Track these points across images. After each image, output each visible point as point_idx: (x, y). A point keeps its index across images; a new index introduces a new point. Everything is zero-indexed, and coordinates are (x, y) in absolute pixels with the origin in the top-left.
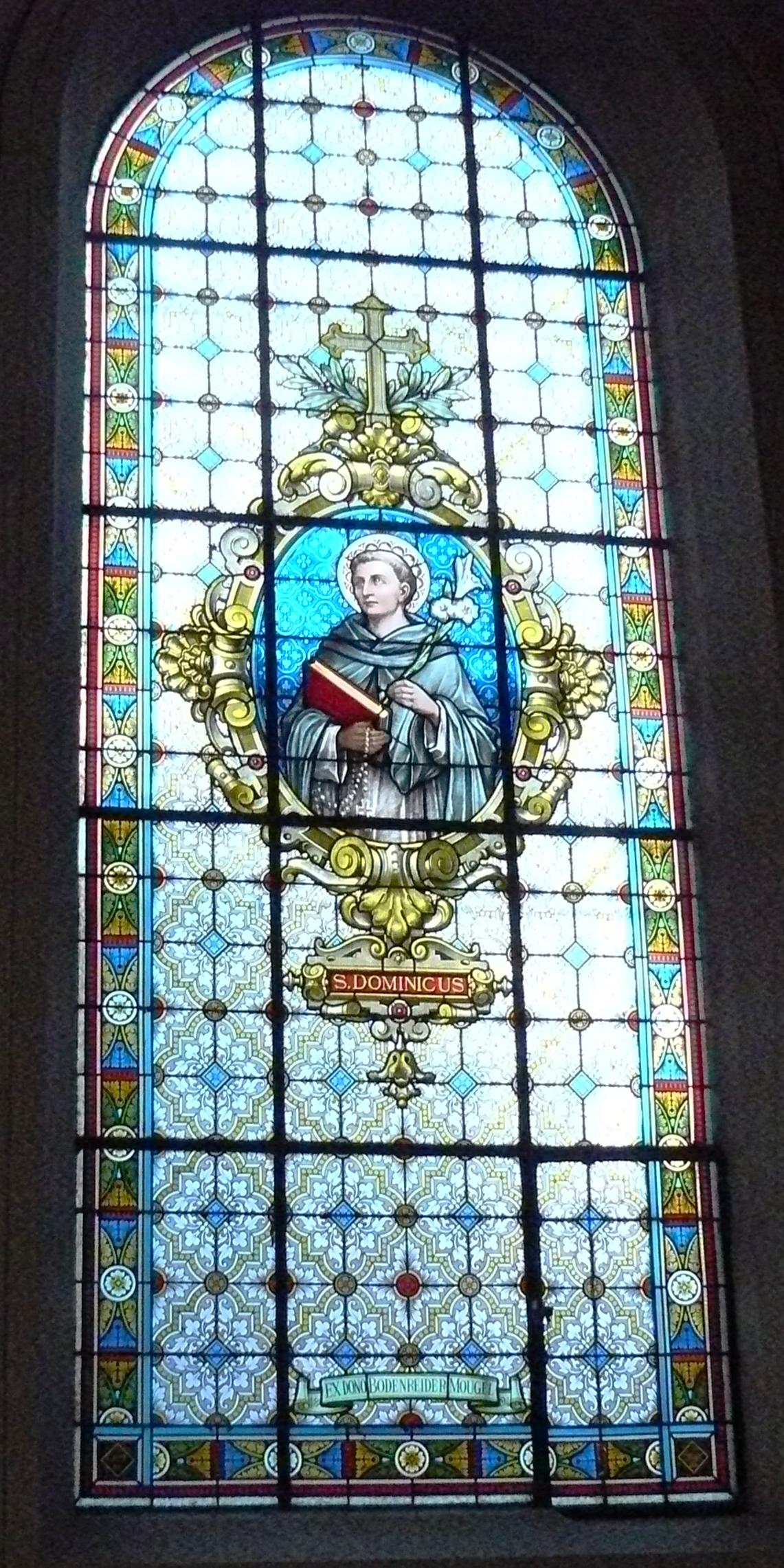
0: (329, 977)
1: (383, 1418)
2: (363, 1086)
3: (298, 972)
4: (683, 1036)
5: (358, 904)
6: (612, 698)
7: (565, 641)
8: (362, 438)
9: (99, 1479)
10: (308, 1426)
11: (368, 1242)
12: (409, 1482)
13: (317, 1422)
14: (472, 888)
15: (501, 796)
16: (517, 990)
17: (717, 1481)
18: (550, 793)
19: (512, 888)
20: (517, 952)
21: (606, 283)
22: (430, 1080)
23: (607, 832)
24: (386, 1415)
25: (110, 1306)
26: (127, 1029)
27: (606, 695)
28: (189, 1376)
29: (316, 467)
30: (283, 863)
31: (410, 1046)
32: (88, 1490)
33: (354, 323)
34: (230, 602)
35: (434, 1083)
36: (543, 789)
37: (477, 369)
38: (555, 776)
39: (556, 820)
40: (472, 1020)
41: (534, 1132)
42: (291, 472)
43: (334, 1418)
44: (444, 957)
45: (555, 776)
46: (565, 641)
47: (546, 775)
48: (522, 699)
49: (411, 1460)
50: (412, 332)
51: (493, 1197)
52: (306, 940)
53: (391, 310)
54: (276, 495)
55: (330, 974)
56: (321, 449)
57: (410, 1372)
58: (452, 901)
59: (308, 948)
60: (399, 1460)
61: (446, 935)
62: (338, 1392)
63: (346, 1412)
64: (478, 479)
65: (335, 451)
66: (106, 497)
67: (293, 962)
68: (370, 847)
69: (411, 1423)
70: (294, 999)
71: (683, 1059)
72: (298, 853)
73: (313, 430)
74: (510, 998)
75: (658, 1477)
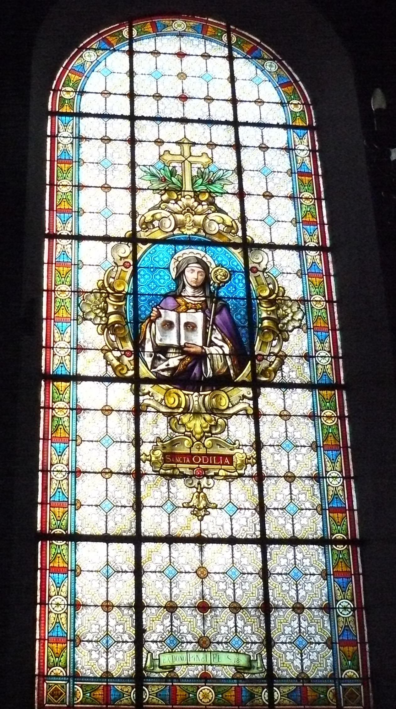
6: (304, 322)
7: (281, 294)
13: (157, 675)
14: (236, 414)
27: (301, 320)
29: (158, 216)
33: (176, 149)
36: (270, 365)
48: (259, 323)
54: (138, 228)
57: (205, 651)
60: (200, 695)
61: (224, 435)
62: (166, 660)
63: (172, 671)
69: (205, 678)
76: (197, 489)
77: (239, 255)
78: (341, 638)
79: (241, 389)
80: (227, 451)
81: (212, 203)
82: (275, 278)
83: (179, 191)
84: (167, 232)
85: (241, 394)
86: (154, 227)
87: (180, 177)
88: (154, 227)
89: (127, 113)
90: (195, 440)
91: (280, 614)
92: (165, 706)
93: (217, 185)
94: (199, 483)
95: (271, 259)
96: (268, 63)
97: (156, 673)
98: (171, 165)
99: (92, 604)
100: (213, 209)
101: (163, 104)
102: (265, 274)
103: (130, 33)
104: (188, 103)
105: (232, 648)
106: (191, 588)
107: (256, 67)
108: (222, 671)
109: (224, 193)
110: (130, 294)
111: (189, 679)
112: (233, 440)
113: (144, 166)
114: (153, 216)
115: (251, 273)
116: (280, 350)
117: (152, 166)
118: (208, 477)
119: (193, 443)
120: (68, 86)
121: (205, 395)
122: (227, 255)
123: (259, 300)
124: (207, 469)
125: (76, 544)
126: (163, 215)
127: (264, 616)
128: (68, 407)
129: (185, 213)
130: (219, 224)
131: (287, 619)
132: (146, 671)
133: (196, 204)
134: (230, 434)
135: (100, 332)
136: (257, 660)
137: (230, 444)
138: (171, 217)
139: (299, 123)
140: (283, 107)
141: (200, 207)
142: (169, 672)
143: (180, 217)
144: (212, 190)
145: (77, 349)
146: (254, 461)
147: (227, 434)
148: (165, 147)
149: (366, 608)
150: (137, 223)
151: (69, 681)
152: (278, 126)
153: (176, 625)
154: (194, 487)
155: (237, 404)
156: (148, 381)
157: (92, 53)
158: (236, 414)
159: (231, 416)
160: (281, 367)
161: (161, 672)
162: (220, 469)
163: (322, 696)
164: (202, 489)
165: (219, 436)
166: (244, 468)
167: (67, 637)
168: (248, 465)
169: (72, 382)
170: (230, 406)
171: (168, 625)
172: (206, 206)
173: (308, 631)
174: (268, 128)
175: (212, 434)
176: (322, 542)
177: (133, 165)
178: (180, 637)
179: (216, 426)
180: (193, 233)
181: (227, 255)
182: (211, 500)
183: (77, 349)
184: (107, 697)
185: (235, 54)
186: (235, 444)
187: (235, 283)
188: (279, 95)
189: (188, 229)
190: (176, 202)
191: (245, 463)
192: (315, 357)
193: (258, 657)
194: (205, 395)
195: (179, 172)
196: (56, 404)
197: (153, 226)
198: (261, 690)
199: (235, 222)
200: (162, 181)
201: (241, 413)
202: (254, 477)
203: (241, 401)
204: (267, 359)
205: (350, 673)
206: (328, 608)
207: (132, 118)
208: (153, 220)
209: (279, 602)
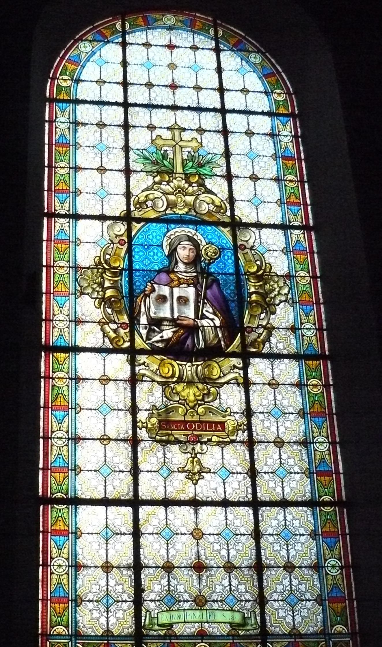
6: (290, 296)
7: (268, 270)
8: (171, 184)
13: (155, 633)
14: (228, 383)
20: (249, 413)
24: (192, 629)
29: (151, 197)
33: (167, 134)
36: (259, 337)
42: (139, 198)
54: (132, 208)
59: (149, 410)
61: (216, 403)
62: (164, 618)
76: (191, 454)
77: (227, 233)
80: (219, 418)
81: (202, 185)
82: (262, 255)
84: (160, 212)
85: (232, 364)
86: (147, 207)
88: (147, 207)
89: (121, 100)
90: (188, 408)
93: (206, 168)
94: (193, 449)
95: (258, 237)
97: (155, 631)
98: (163, 149)
99: (92, 565)
100: (202, 191)
102: (253, 252)
108: (218, 628)
109: (213, 176)
112: (225, 408)
114: (146, 196)
115: (239, 251)
116: (268, 323)
117: (145, 150)
119: (187, 410)
122: (216, 233)
124: (201, 435)
125: (76, 508)
126: (156, 196)
130: (208, 204)
133: (186, 185)
136: (251, 617)
137: (222, 411)
139: (282, 111)
140: (267, 96)
141: (191, 188)
142: (167, 630)
143: (172, 198)
147: (219, 402)
148: (157, 132)
149: (353, 566)
150: (132, 203)
151: (71, 640)
152: (263, 113)
153: (173, 585)
154: (188, 452)
156: (143, 352)
157: (87, 44)
158: (228, 383)
159: (222, 384)
161: (160, 630)
164: (196, 454)
165: (211, 404)
166: (236, 434)
170: (222, 375)
172: (196, 188)
174: (254, 116)
175: (205, 402)
177: (127, 148)
179: (209, 394)
180: (184, 213)
182: (205, 464)
185: (222, 46)
186: (226, 411)
194: (198, 365)
197: (147, 205)
199: (224, 202)
201: (232, 382)
203: (232, 371)
204: (255, 332)
205: (340, 628)
208: (147, 201)
209: (271, 562)
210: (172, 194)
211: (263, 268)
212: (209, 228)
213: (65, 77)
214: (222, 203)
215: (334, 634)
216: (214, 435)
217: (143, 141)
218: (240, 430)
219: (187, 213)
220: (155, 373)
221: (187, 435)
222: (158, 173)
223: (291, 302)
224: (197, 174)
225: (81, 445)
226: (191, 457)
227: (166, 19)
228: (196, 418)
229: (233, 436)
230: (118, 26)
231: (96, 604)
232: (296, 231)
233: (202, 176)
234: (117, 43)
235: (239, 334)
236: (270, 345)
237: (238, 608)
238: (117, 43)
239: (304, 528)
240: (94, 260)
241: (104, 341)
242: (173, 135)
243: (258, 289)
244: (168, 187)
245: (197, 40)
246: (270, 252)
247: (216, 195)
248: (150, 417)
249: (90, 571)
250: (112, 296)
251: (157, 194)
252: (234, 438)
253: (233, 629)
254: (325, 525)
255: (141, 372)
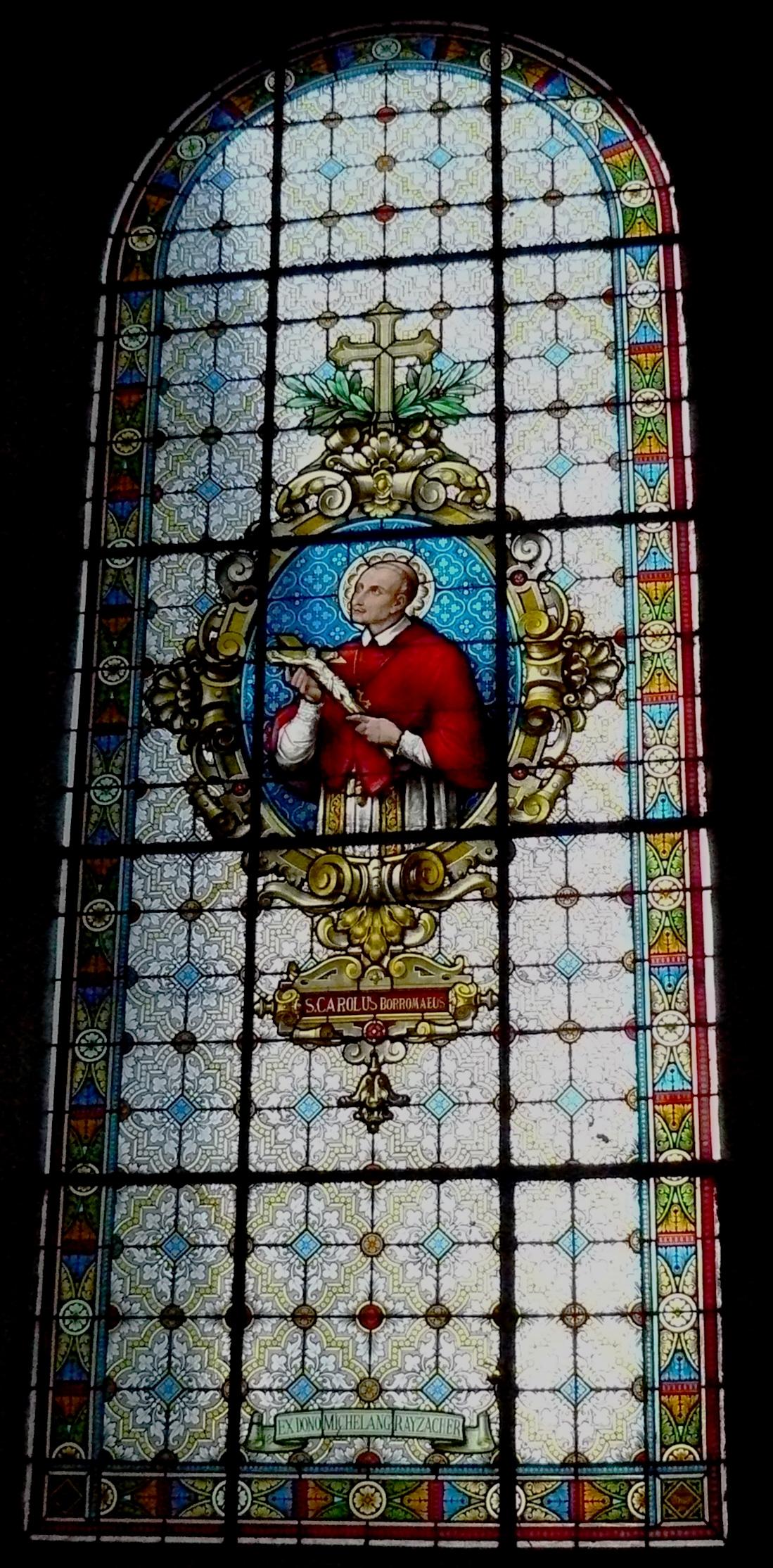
0: (302, 1001)
1: (337, 1456)
2: (333, 1112)
3: (270, 998)
4: (689, 1044)
5: (335, 926)
6: (621, 685)
7: (574, 627)
8: (366, 450)
9: (49, 1515)
10: (260, 1464)
11: (330, 1272)
12: (364, 1523)
13: (269, 1459)
14: (459, 899)
15: (494, 800)
16: (502, 1003)
17: (709, 1525)
18: (549, 789)
19: (502, 899)
20: (504, 965)
21: (637, 250)
22: (405, 1102)
23: (610, 827)
24: (345, 1452)
25: (67, 1339)
26: (679, 1050)
27: (616, 681)
28: (140, 1411)
29: (317, 485)
30: (260, 888)
31: (385, 1069)
32: (38, 1524)
33: (361, 331)
34: (223, 629)
35: (408, 1105)
36: (541, 787)
37: (493, 360)
38: (553, 774)
39: (554, 818)
40: (450, 1038)
41: (515, 1152)
42: (291, 491)
43: (287, 1456)
44: (424, 972)
45: (553, 774)
46: (574, 627)
47: (546, 773)
48: (522, 694)
49: (368, 1500)
50: (425, 333)
51: (335, 1223)
52: (280, 965)
53: (404, 313)
54: (274, 516)
55: (303, 997)
56: (323, 467)
57: (369, 1408)
58: (436, 914)
59: (282, 973)
60: (355, 1501)
61: (430, 950)
62: (291, 1429)
63: (300, 1450)
64: (487, 475)
65: (339, 468)
66: (671, 530)
67: (267, 986)
68: (350, 864)
69: (367, 1463)
70: (264, 1026)
71: (687, 1068)
72: (275, 878)
73: (314, 446)
74: (496, 1011)
75: (639, 1521)
76: (369, 1066)
77: (485, 549)
78: (665, 1376)
79: (470, 843)
80: (436, 981)
81: (431, 442)
82: (564, 592)
83: (365, 424)
84: (334, 518)
85: (470, 854)
86: (307, 510)
87: (368, 392)
88: (307, 510)
90: (367, 963)
91: (398, 1329)
92: (560, 1525)
93: (450, 400)
94: (374, 1054)
95: (557, 549)
96: (581, 104)
97: (268, 1453)
98: (351, 368)
99: (406, 1313)
100: (436, 456)
101: (451, 222)
102: (542, 585)
103: (280, 83)
104: (396, 222)
105: (427, 1401)
106: (480, 1275)
107: (553, 117)
108: (403, 1449)
109: (464, 417)
110: (250, 662)
111: (334, 1465)
112: (450, 958)
113: (293, 376)
114: (307, 485)
115: (511, 587)
116: (565, 753)
117: (310, 375)
118: (394, 1040)
119: (364, 969)
120: (145, 223)
121: (394, 864)
122: (460, 551)
123: (525, 644)
124: (393, 1023)
126: (328, 482)
127: (231, 1335)
128: (681, 887)
129: (377, 470)
130: (445, 486)
131: (412, 1339)
132: (248, 1450)
133: (399, 448)
134: (445, 942)
135: (183, 748)
136: (478, 1426)
137: (445, 965)
138: (346, 485)
139: (641, 231)
140: (607, 201)
141: (409, 453)
142: (295, 1451)
143: (365, 480)
144: (438, 414)
145: (630, 762)
146: (495, 998)
147: (436, 946)
148: (341, 328)
150: (273, 503)
152: (590, 245)
153: (178, 1355)
154: (363, 1062)
155: (463, 876)
156: (277, 842)
157: (197, 140)
158: (459, 899)
159: (449, 904)
160: (565, 788)
161: (278, 1452)
162: (420, 1022)
163: (336, 1499)
164: (379, 1066)
165: (420, 949)
166: (473, 1014)
167: (700, 1380)
168: (481, 1009)
169: (686, 832)
170: (447, 882)
171: (294, 1355)
172: (423, 451)
173: (186, 1364)
174: (569, 254)
175: (407, 947)
176: (120, 1179)
177: (270, 378)
178: (320, 1379)
179: (415, 925)
180: (391, 513)
181: (460, 551)
182: (397, 1088)
183: (630, 762)
184: (577, 1504)
186: (453, 965)
187: (304, 621)
188: (598, 174)
189: (380, 506)
190: (358, 448)
191: (475, 1004)
192: (642, 762)
193: (482, 1419)
194: (394, 864)
195: (368, 380)
196: (655, 881)
197: (306, 506)
198: (347, 1487)
199: (484, 478)
200: (330, 406)
201: (469, 896)
202: (516, 1033)
203: (472, 870)
204: (534, 775)
205: (680, 1450)
206: (643, 1315)
207: (498, 255)
208: (307, 495)
209: (266, 1305)
210: (367, 472)
211: (564, 624)
212: (443, 542)
213: (144, 229)
214: (480, 479)
215: (669, 1463)
216: (423, 1020)
217: (306, 355)
218: (484, 1004)
219: (396, 514)
220: (299, 888)
221: (361, 1024)
222: (335, 428)
223: (622, 699)
224: (427, 418)
225: (624, 1017)
226: (369, 1072)
227: (379, 50)
228: (385, 984)
229: (464, 1019)
230: (269, 82)
231: (144, 1395)
232: (649, 525)
233: (437, 422)
234: (265, 126)
235: (495, 785)
236: (567, 805)
237: (451, 1406)
238: (265, 126)
239: (347, 1228)
240: (184, 645)
241: (194, 824)
242: (377, 328)
243: (547, 674)
244: (358, 457)
245: (447, 86)
246: (584, 583)
247: (467, 463)
248: (282, 989)
249: (401, 1325)
250: (214, 725)
251: (332, 478)
252: (467, 1023)
253: (436, 1451)
254: (667, 1215)
255: (272, 888)
